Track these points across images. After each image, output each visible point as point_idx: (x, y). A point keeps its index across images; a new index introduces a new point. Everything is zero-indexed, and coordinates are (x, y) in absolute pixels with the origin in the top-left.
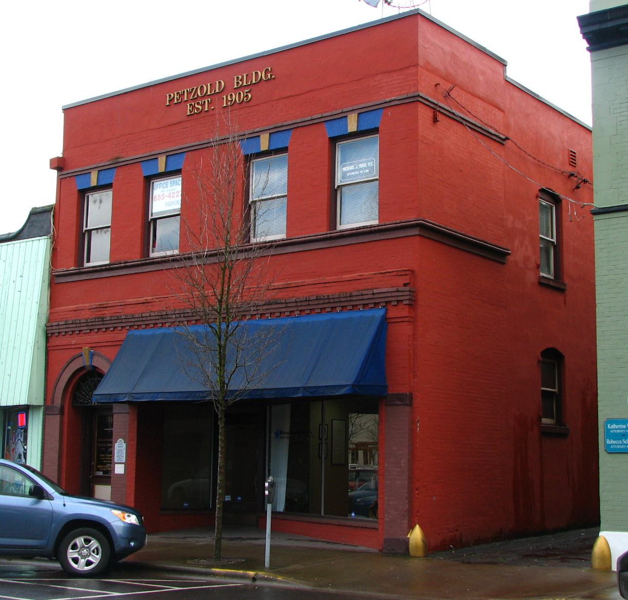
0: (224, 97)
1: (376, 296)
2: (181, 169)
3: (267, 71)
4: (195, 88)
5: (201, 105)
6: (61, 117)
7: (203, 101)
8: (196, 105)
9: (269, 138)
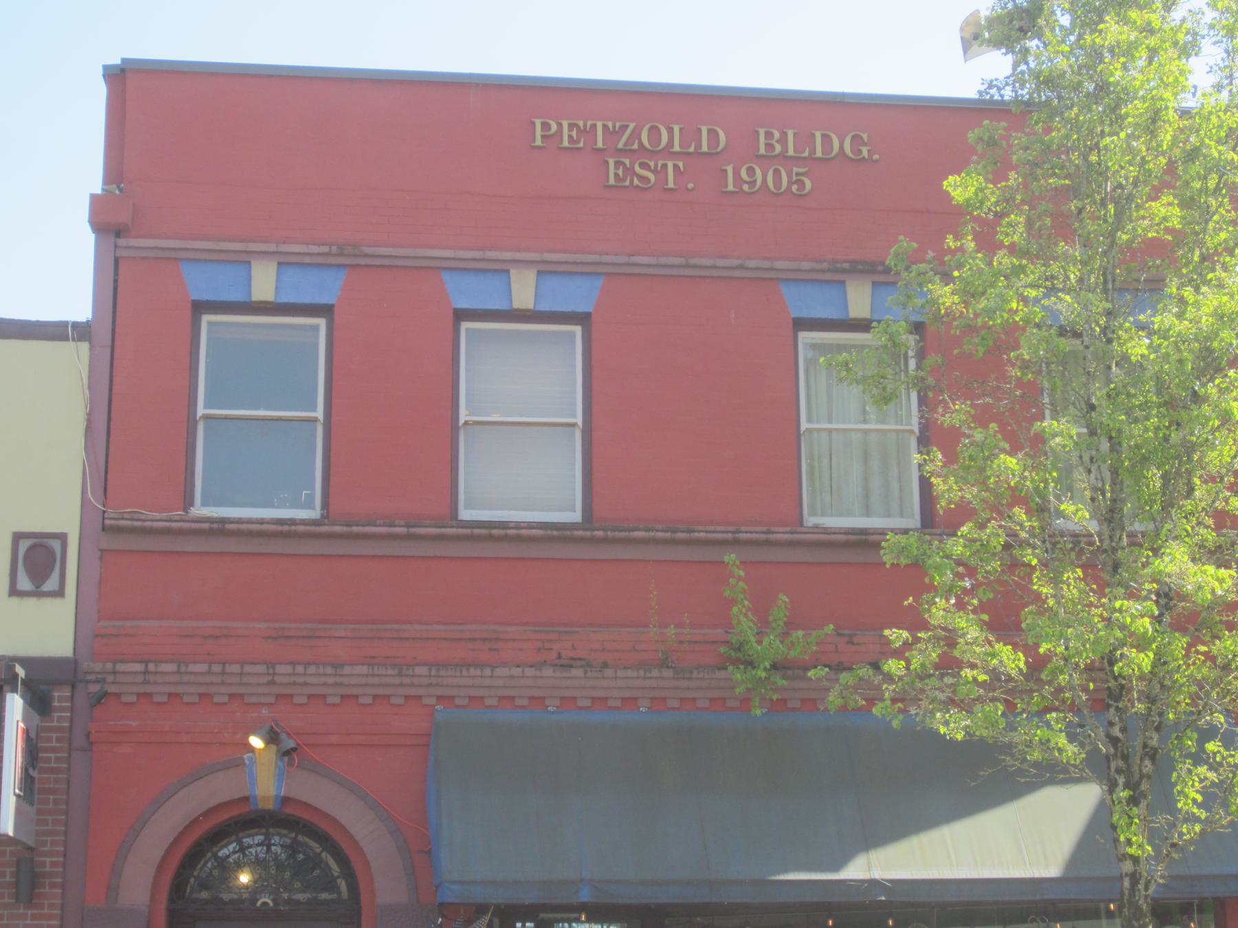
0: (730, 169)
1: (120, 678)
2: (332, 306)
3: (856, 139)
4: (632, 126)
5: (655, 171)
6: (99, 93)
7: (660, 163)
8: (637, 168)
9: (278, 281)
